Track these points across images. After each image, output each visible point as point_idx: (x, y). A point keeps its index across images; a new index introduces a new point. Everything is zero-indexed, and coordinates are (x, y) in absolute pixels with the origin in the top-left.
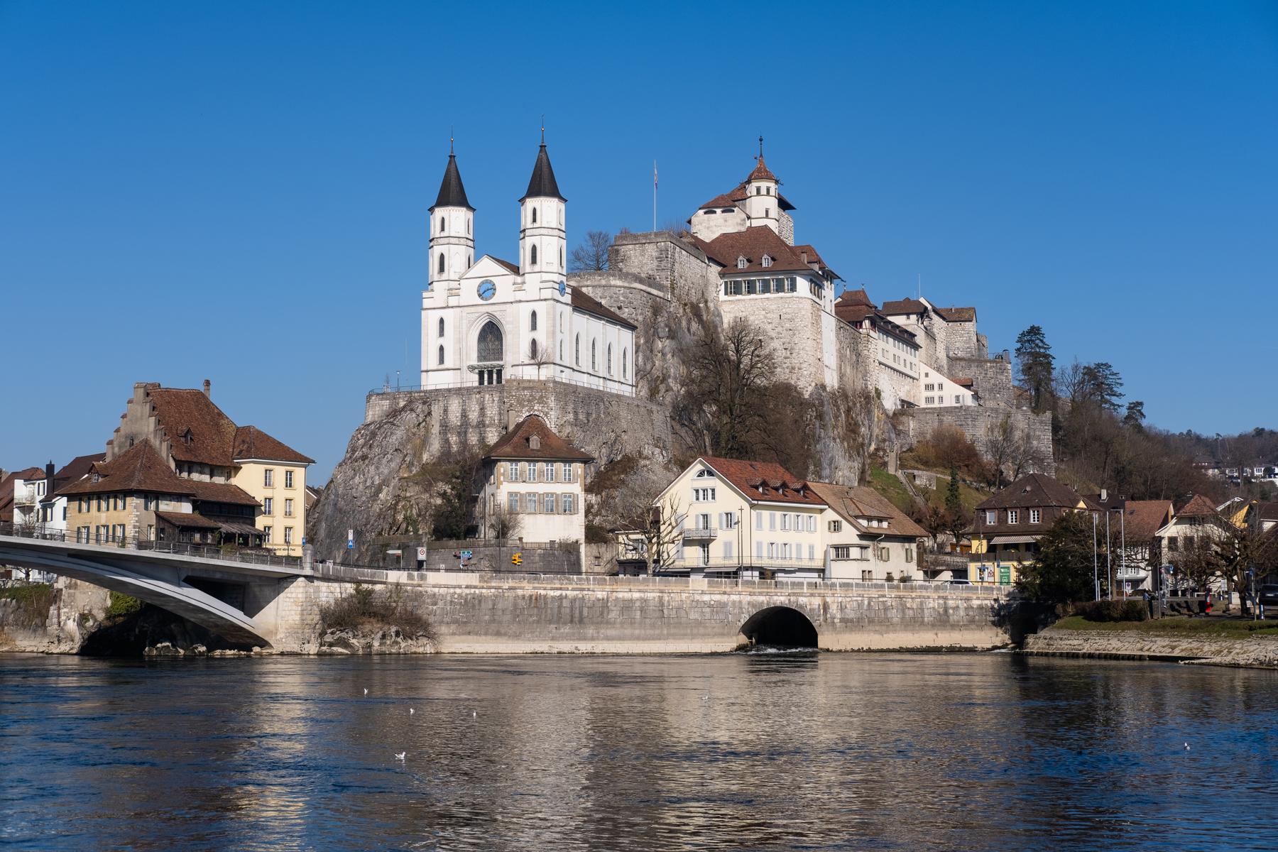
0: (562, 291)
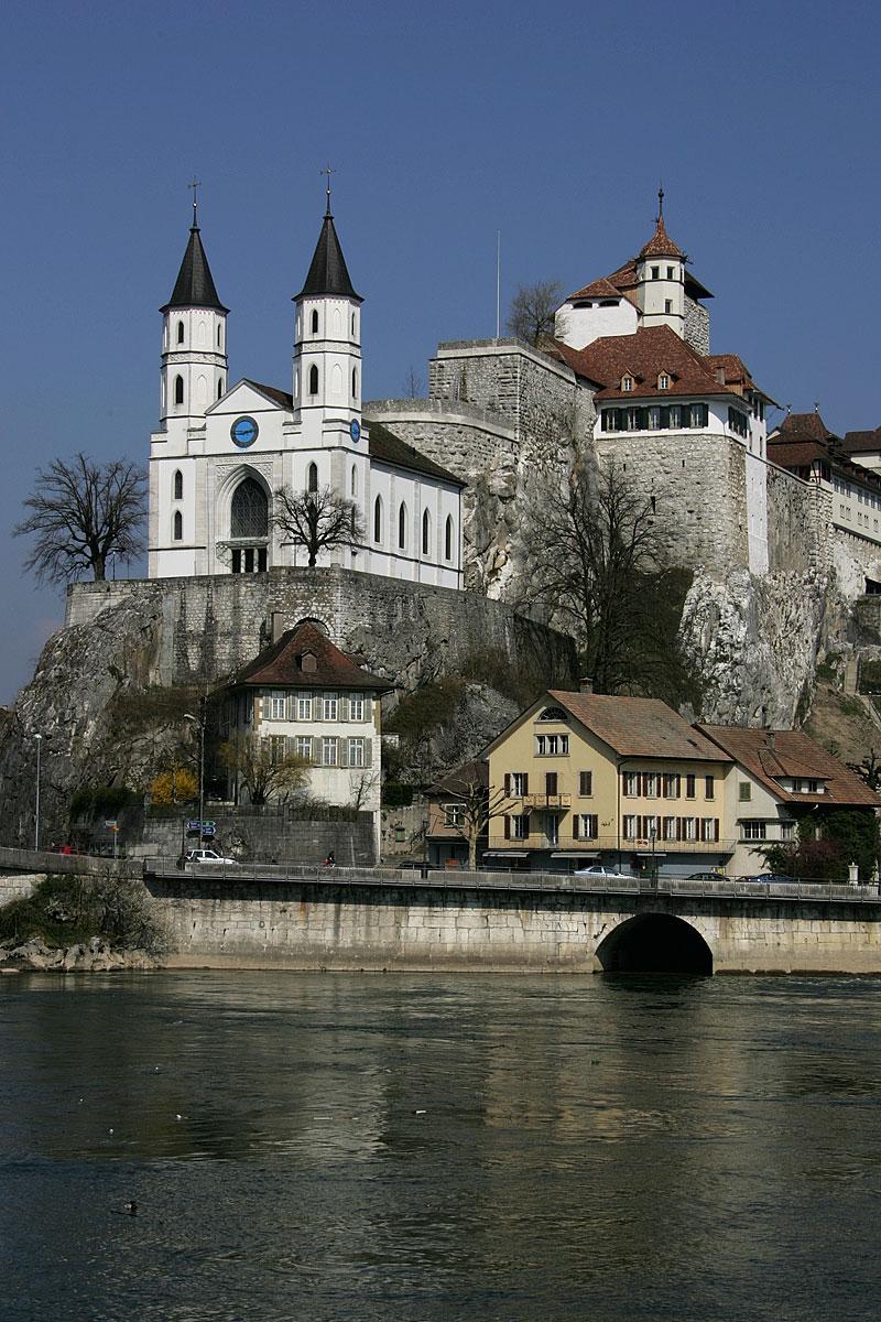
0: (355, 436)
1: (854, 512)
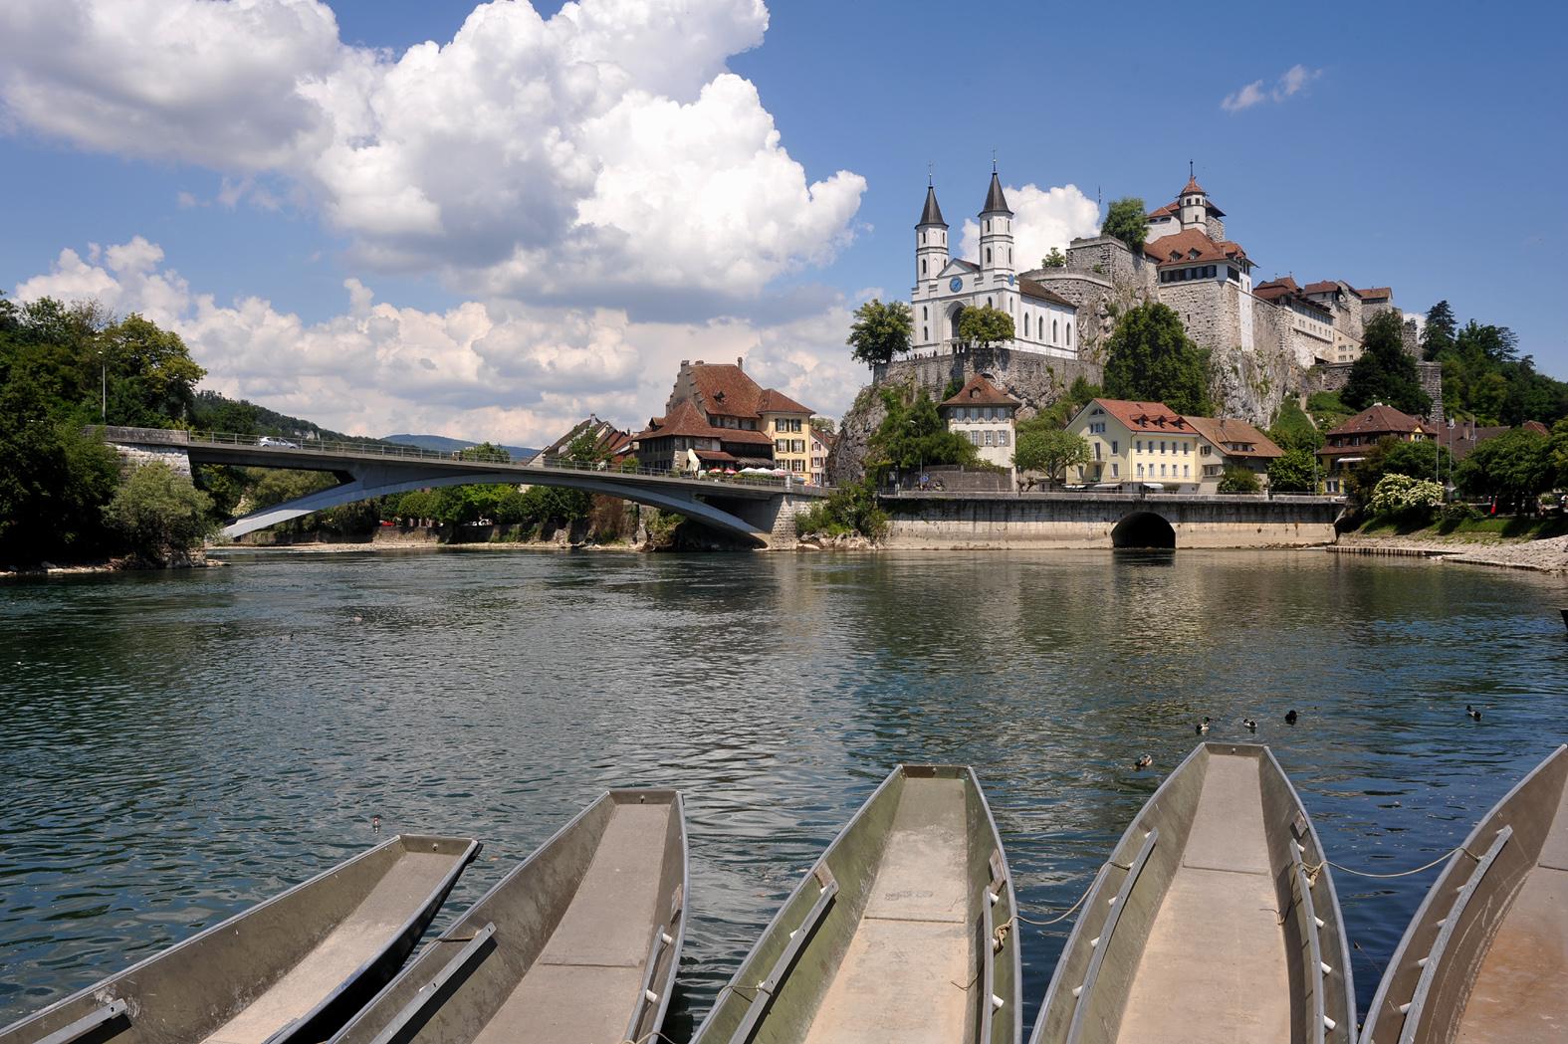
1: (1307, 324)
